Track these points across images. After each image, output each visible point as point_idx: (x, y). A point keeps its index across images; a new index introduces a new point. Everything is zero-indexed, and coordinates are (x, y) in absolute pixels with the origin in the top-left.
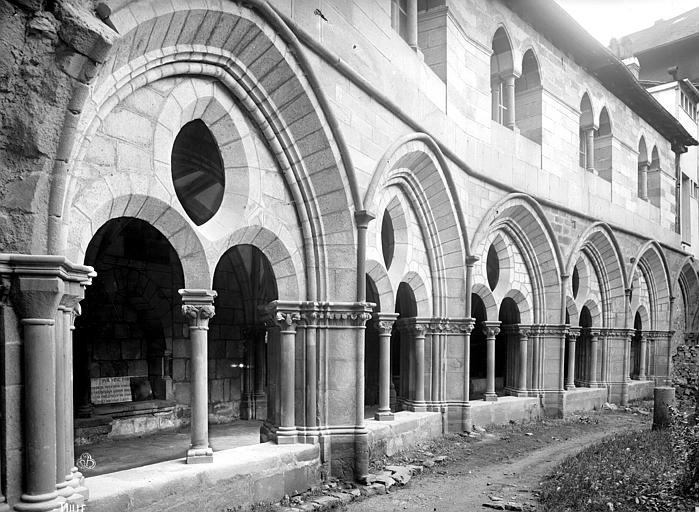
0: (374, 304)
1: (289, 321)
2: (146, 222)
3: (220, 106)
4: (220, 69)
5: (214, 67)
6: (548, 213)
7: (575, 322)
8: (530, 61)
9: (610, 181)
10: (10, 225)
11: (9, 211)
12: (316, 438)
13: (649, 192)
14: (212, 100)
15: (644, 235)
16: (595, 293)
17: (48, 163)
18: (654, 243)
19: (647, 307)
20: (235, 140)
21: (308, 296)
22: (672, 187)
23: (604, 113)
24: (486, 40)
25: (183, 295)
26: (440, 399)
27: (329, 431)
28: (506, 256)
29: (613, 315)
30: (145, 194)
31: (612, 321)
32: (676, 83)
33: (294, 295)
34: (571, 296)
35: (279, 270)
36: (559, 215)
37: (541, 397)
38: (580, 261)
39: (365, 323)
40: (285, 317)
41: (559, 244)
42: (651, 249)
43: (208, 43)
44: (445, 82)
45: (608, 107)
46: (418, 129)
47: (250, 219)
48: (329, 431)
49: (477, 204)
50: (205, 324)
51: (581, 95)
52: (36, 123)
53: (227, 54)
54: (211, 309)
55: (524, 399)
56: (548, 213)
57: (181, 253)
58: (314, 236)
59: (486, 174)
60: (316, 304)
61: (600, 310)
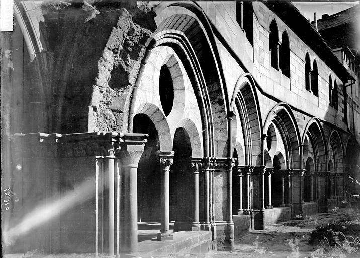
0: (236, 159)
1: (197, 167)
2: (148, 116)
3: (175, 59)
4: (178, 41)
5: (176, 40)
6: (294, 112)
7: (270, 166)
8: (285, 35)
9: (318, 96)
10: (113, 118)
11: (113, 111)
12: (210, 228)
13: (312, 85)
14: (173, 56)
15: (311, 114)
16: (311, 153)
17: (131, 88)
18: (316, 119)
19: (333, 160)
20: (180, 76)
21: (205, 154)
22: (342, 100)
23: (315, 62)
24: (268, 26)
25: (159, 154)
26: (210, 221)
27: (216, 224)
28: (274, 134)
29: (320, 165)
30: (151, 102)
31: (320, 168)
32: (341, 49)
33: (199, 154)
34: (267, 149)
35: (193, 141)
36: (299, 113)
37: (291, 207)
38: (271, 126)
39: (231, 168)
40: (195, 165)
41: (299, 128)
42: (314, 123)
43: (177, 29)
44: (253, 46)
45: (316, 60)
46: (246, 71)
47: (185, 116)
48: (216, 224)
49: (266, 107)
50: (168, 168)
51: (305, 54)
52: (129, 68)
53: (182, 34)
54: (172, 161)
55: (312, 203)
56: (294, 112)
57: (159, 132)
58: (208, 124)
59: (270, 94)
60: (210, 158)
61: (314, 162)
